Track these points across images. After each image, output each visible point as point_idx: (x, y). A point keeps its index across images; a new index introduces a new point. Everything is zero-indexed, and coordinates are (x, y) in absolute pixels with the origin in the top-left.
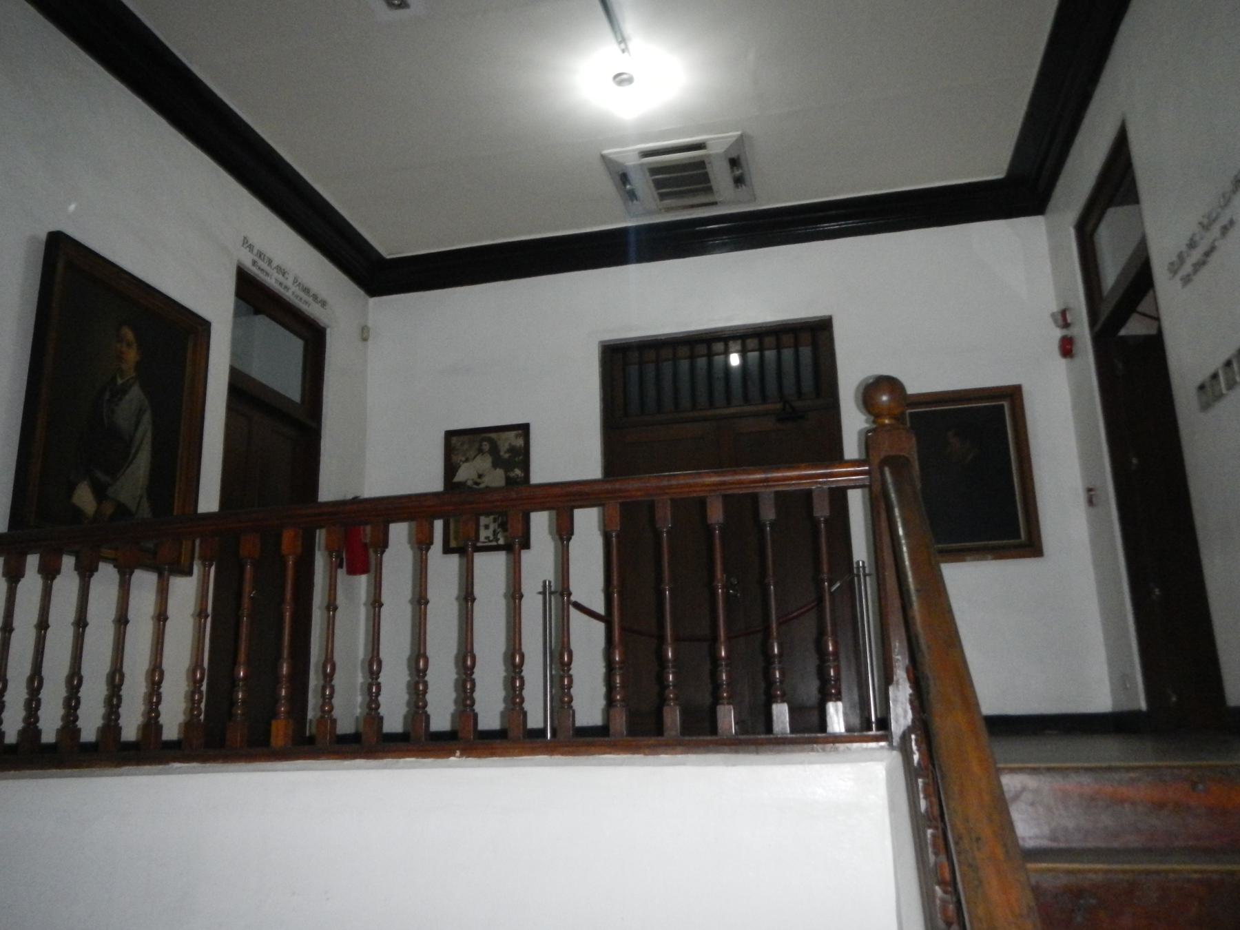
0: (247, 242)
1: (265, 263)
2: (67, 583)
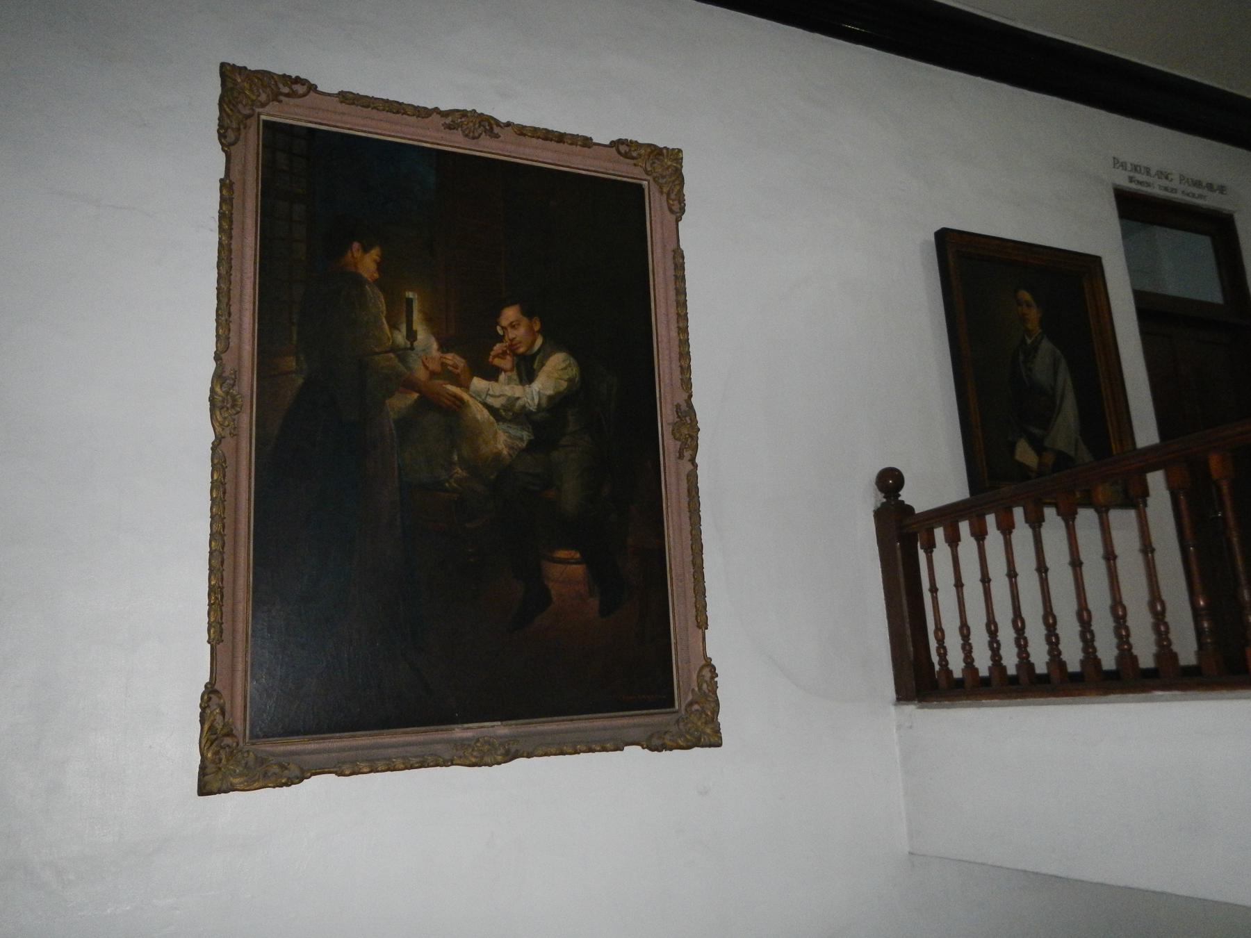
0: (1118, 162)
1: (1143, 174)
2: (1022, 533)
